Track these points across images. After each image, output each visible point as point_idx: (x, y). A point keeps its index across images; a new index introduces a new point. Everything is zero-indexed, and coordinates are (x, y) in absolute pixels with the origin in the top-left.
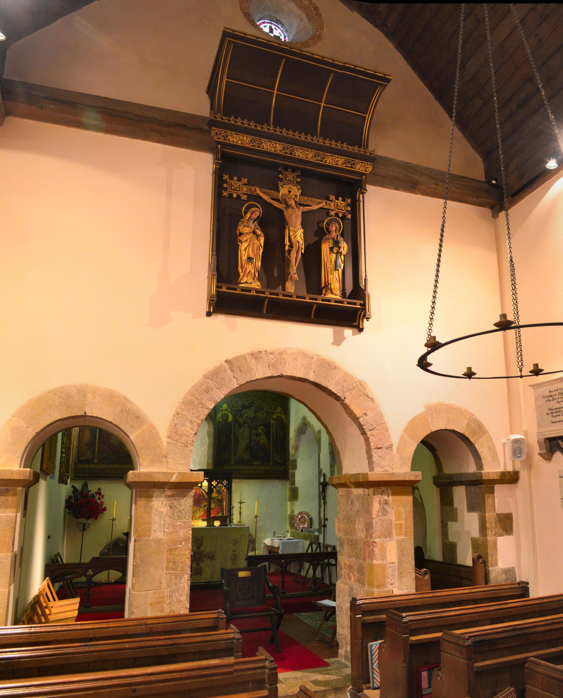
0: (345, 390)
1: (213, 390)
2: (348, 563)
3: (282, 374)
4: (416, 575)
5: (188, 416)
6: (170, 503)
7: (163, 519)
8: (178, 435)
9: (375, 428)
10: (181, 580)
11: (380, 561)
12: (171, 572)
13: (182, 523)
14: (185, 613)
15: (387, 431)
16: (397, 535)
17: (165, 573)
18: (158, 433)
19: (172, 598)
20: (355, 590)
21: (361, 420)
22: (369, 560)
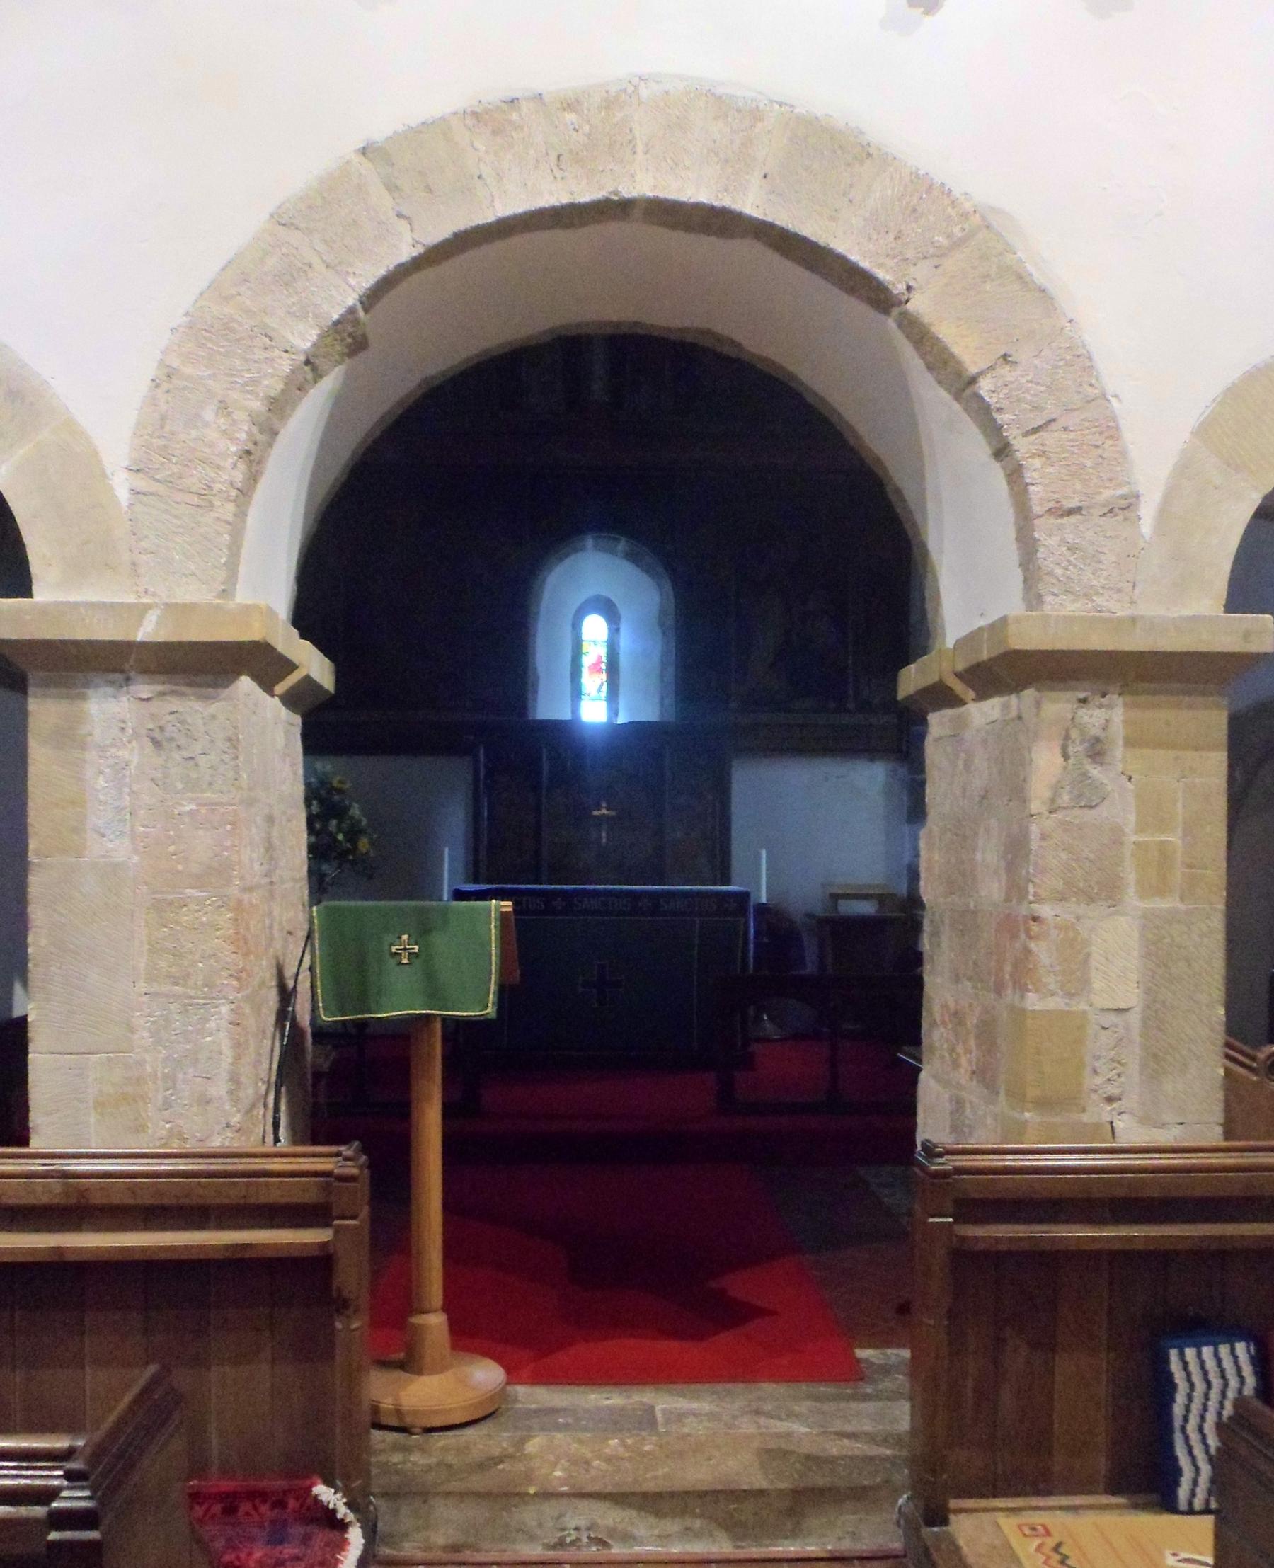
0: (910, 254)
1: (310, 275)
2: (952, 1005)
3: (615, 193)
4: (1227, 1070)
5: (211, 382)
6: (151, 726)
7: (126, 790)
8: (174, 460)
9: (1054, 420)
10: (204, 1020)
11: (1056, 998)
12: (165, 988)
13: (198, 805)
14: (227, 1144)
15: (1111, 430)
16: (1144, 892)
17: (144, 990)
18: (95, 453)
19: (174, 1088)
20: (968, 1111)
21: (985, 387)
22: (1015, 993)
